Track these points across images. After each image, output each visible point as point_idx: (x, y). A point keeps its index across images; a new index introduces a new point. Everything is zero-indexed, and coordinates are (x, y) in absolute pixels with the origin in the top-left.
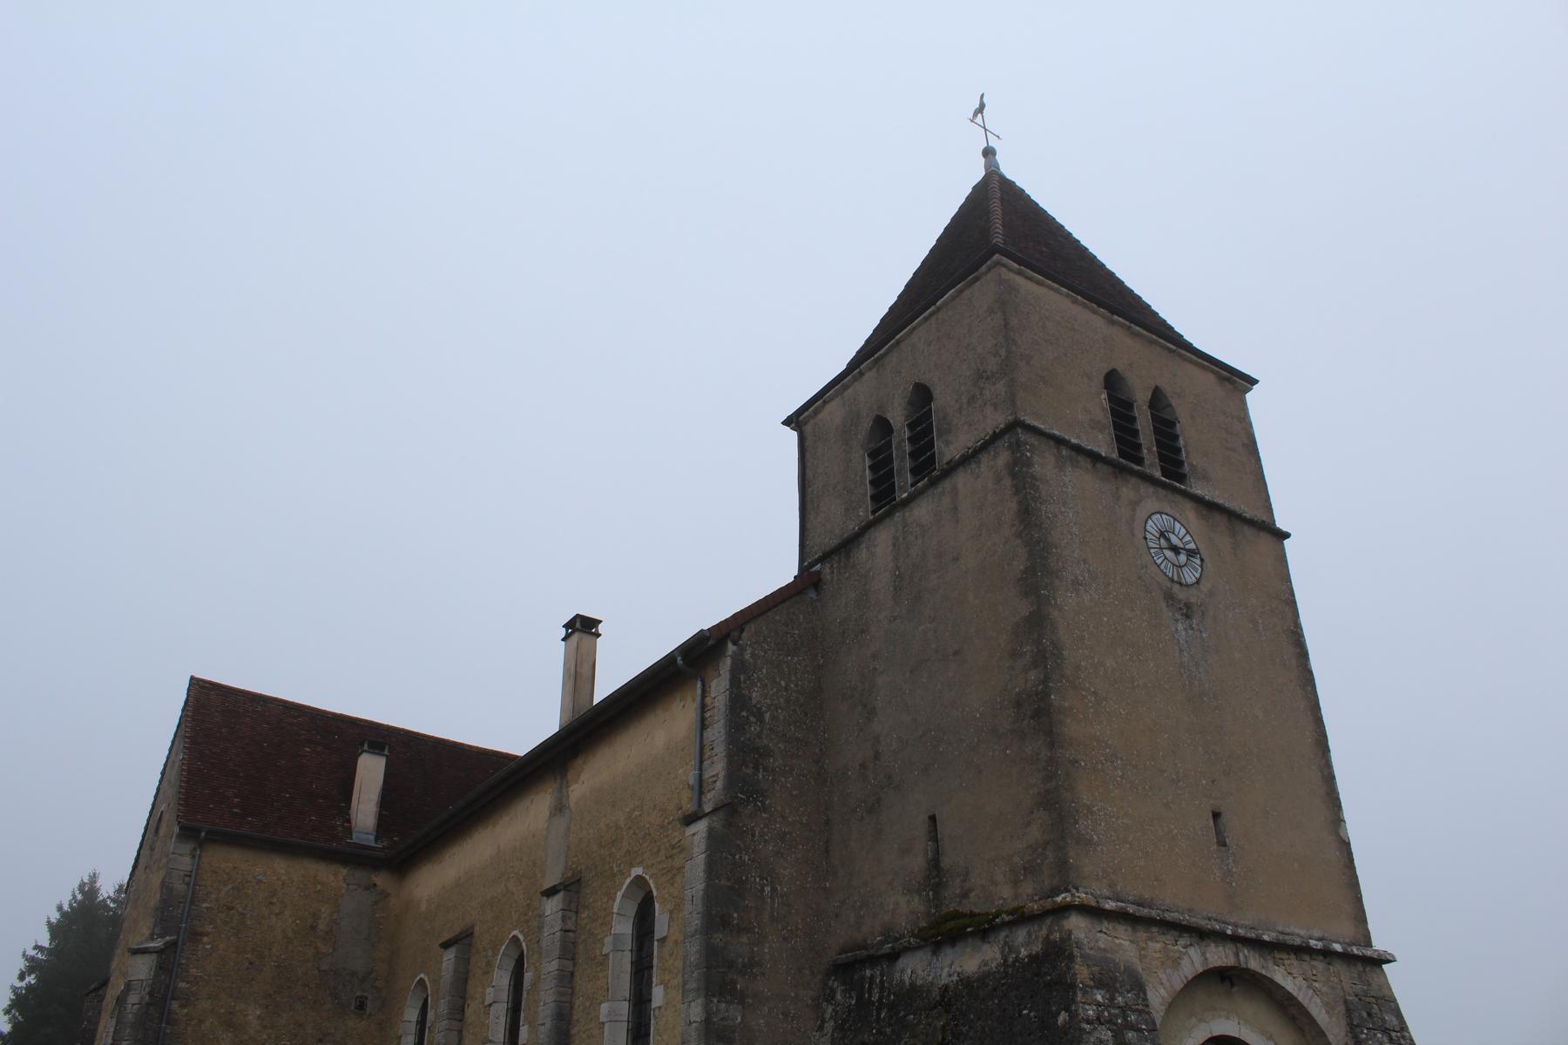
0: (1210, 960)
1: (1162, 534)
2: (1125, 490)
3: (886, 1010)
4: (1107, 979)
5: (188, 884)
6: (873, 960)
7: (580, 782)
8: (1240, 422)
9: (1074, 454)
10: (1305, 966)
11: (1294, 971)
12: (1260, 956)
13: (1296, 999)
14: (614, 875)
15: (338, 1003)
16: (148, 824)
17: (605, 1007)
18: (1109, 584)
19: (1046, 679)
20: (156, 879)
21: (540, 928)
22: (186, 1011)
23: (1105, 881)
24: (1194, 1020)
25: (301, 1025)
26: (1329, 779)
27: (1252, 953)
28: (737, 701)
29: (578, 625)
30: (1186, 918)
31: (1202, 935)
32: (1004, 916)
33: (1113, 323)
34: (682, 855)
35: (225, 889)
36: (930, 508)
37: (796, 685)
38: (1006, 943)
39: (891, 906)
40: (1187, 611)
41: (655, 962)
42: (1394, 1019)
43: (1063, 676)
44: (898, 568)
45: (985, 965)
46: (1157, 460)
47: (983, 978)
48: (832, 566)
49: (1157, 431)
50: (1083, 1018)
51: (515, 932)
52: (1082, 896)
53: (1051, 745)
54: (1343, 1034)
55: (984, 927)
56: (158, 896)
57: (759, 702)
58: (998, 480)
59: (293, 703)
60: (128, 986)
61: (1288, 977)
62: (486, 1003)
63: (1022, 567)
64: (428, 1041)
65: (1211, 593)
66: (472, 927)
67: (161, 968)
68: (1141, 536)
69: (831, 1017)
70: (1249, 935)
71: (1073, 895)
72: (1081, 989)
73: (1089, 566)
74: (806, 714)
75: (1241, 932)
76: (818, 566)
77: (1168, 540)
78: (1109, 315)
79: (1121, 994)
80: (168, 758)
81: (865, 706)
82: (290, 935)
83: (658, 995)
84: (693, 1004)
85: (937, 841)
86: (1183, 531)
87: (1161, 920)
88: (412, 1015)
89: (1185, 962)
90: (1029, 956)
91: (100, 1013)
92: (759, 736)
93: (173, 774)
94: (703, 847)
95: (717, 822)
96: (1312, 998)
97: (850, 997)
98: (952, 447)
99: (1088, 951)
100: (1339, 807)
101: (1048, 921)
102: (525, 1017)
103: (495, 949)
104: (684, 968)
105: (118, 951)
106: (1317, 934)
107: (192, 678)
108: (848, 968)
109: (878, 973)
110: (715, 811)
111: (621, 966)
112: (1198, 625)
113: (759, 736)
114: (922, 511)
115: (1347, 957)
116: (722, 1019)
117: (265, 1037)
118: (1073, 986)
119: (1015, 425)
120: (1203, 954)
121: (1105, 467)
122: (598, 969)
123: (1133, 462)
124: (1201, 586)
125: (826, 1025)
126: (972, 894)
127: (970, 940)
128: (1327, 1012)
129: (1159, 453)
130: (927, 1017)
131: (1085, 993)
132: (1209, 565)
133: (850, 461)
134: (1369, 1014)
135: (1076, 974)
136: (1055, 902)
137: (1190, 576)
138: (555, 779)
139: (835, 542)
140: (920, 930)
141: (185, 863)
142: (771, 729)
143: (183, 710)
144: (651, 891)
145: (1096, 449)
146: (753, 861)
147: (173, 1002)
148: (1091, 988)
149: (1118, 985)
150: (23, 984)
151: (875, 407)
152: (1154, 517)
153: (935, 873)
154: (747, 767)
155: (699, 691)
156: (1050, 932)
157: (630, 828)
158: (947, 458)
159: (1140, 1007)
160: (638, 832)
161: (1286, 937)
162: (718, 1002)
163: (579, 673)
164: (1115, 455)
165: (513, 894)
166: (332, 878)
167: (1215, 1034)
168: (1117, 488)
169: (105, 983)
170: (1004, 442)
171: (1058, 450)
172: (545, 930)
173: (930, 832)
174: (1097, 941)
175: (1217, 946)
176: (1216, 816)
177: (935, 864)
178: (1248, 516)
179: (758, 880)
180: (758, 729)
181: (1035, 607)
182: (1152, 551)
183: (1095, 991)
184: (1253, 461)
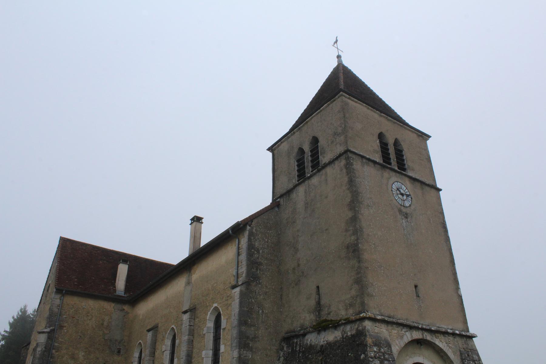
0: (414, 336)
1: (398, 189)
2: (385, 174)
3: (301, 354)
4: (378, 343)
5: (59, 309)
6: (297, 336)
7: (196, 274)
8: (425, 151)
10: (446, 338)
11: (442, 340)
12: (431, 335)
14: (207, 306)
17: (204, 353)
19: (357, 239)
20: (47, 307)
21: (182, 325)
22: (57, 353)
24: (408, 357)
26: (455, 274)
27: (428, 334)
28: (251, 247)
29: (195, 219)
30: (405, 322)
31: (411, 328)
32: (342, 321)
33: (381, 116)
34: (231, 299)
35: (72, 311)
37: (271, 241)
38: (343, 330)
39: (303, 318)
40: (406, 216)
41: (221, 337)
46: (396, 164)
47: (335, 343)
49: (396, 154)
51: (173, 326)
52: (369, 314)
53: (359, 262)
55: (335, 325)
56: (48, 313)
57: (258, 246)
58: (341, 170)
61: (440, 342)
62: (163, 351)
66: (158, 324)
68: (390, 190)
69: (282, 356)
70: (427, 328)
71: (366, 314)
72: (369, 346)
74: (274, 251)
75: (424, 327)
76: (279, 200)
77: (400, 191)
79: (383, 348)
80: (52, 265)
81: (295, 248)
82: (94, 327)
83: (222, 348)
84: (234, 351)
85: (319, 295)
86: (405, 188)
87: (397, 322)
88: (137, 355)
89: (405, 337)
90: (351, 335)
91: (27, 354)
92: (258, 258)
93: (54, 271)
94: (238, 297)
95: (243, 288)
97: (289, 349)
99: (371, 333)
104: (231, 339)
105: (34, 333)
106: (450, 327)
109: (299, 341)
110: (242, 284)
111: (210, 338)
113: (258, 258)
114: (315, 180)
115: (461, 336)
118: (366, 345)
119: (347, 151)
120: (411, 334)
122: (201, 339)
123: (387, 164)
125: (281, 359)
126: (332, 314)
127: (331, 329)
128: (454, 355)
130: (316, 356)
131: (370, 348)
134: (468, 355)
135: (367, 341)
136: (360, 316)
137: (407, 204)
139: (285, 191)
140: (314, 326)
141: (58, 302)
143: (58, 248)
144: (220, 312)
145: (375, 160)
148: (372, 346)
149: (382, 345)
151: (299, 144)
152: (395, 183)
153: (319, 306)
155: (237, 243)
156: (358, 327)
158: (323, 162)
159: (389, 353)
162: (243, 350)
163: (196, 236)
164: (382, 162)
166: (109, 307)
168: (382, 173)
170: (343, 157)
172: (183, 325)
173: (317, 292)
174: (374, 330)
175: (416, 332)
176: (416, 287)
177: (319, 303)
178: (427, 183)
179: (257, 308)
180: (258, 256)
182: (394, 195)
183: (374, 347)
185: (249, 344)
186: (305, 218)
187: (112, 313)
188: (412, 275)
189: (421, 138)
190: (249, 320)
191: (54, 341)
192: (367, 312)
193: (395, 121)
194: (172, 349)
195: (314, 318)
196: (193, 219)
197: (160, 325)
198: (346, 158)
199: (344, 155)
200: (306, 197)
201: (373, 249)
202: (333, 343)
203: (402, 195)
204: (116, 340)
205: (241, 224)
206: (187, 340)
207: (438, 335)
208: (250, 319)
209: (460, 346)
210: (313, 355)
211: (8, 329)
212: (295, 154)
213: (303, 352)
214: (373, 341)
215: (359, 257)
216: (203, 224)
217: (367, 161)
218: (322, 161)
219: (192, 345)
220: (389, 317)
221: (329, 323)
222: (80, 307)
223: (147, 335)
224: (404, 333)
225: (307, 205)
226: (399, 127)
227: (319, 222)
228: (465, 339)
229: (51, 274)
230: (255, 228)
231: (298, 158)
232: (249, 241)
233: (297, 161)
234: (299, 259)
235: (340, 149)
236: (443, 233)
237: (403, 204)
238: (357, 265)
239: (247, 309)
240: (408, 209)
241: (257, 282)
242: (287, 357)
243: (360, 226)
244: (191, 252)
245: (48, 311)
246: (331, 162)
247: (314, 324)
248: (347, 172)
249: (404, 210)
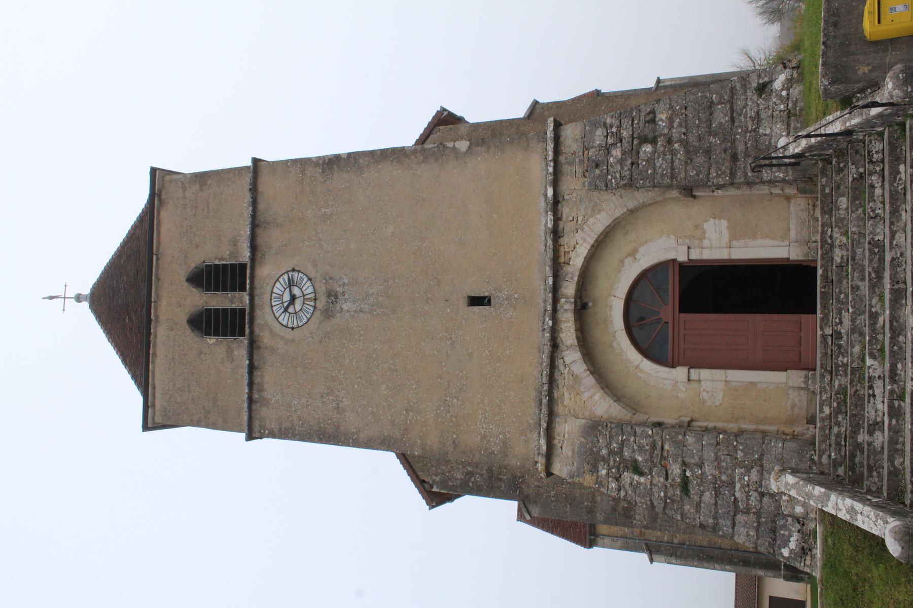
11: (572, 243)
24: (614, 344)
33: (157, 317)
40: (333, 296)
50: (617, 494)
57: (462, 474)
78: (153, 323)
113: (482, 476)
116: (645, 518)
146: (554, 488)
154: (501, 487)
162: (635, 520)
167: (624, 328)
179: (564, 486)
185: (623, 507)
189: (164, 196)
190: (586, 503)
193: (153, 278)
207: (563, 254)
208: (583, 503)
226: (160, 262)
239: (568, 506)
241: (522, 481)
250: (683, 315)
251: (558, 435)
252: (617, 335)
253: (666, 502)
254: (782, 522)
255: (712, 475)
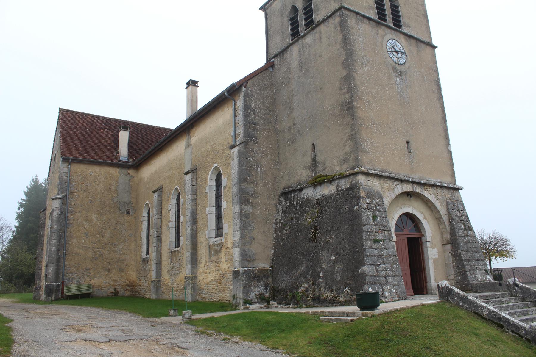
0: (404, 189)
1: (393, 47)
2: (380, 31)
3: (299, 207)
4: (370, 195)
5: (67, 177)
6: (294, 191)
7: (195, 136)
8: (422, 6)
9: (362, 18)
10: (435, 191)
11: (431, 192)
12: (420, 188)
13: (431, 201)
14: (208, 167)
15: (121, 212)
16: (51, 158)
17: (207, 209)
18: (373, 64)
19: (352, 97)
20: (57, 176)
21: (185, 185)
22: (72, 216)
23: (370, 164)
24: (398, 208)
25: (110, 219)
26: (446, 130)
27: (418, 187)
28: (247, 107)
29: (191, 83)
30: (397, 176)
31: (402, 181)
32: (337, 176)
34: (230, 159)
35: (80, 178)
36: (311, 38)
37: (266, 101)
38: (338, 184)
39: (300, 174)
40: (400, 74)
41: (223, 194)
42: (461, 207)
43: (357, 96)
44: (301, 59)
45: (331, 192)
46: (392, 20)
47: (330, 196)
48: (278, 60)
49: (392, 10)
51: (177, 187)
52: (363, 169)
53: (353, 119)
54: (445, 212)
55: (331, 180)
56: (58, 181)
58: (335, 28)
59: (95, 115)
60: (53, 209)
61: (429, 194)
62: (169, 210)
63: (343, 59)
64: (151, 223)
65: (409, 68)
66: (162, 186)
67: (62, 204)
68: (385, 47)
69: (281, 210)
70: (417, 181)
71: (360, 169)
72: (362, 199)
73: (367, 58)
74: (270, 111)
75: (414, 180)
76: (273, 60)
77: (395, 49)
79: (375, 200)
80: (55, 136)
81: (290, 107)
82: (103, 191)
83: (224, 205)
84: (236, 207)
85: (315, 152)
86: (400, 46)
87: (389, 176)
88: (145, 214)
89: (396, 190)
90: (345, 189)
91: (45, 218)
92: (254, 118)
93: (58, 141)
94: (237, 156)
95: (241, 147)
96: (436, 200)
97: (287, 203)
98: (319, 16)
99: (364, 187)
100: (449, 140)
101: (352, 177)
102: (182, 214)
103: (170, 193)
104: (232, 196)
105: (48, 199)
106: (439, 181)
107: (60, 109)
108: (285, 194)
109: (296, 195)
110: (240, 144)
111: (212, 196)
112: (404, 78)
113: (254, 118)
114: (309, 39)
115: (448, 188)
116: (245, 211)
117: (99, 223)
118: (359, 198)
119: (341, 8)
120: (402, 187)
121: (373, 23)
122: (204, 197)
123: (383, 21)
124: (406, 65)
125: (279, 212)
126: (327, 169)
127: (326, 184)
128: (441, 205)
129: (392, 17)
130: (312, 208)
131: (363, 200)
132: (409, 58)
133: (283, 22)
134: (454, 205)
135: (360, 194)
136: (354, 171)
137: (402, 61)
138: (186, 136)
139: (278, 51)
140: (310, 181)
141: (66, 170)
142: (258, 116)
143: (58, 119)
144: (220, 171)
145: (370, 16)
146: (254, 160)
147: (68, 214)
148: (365, 198)
149: (374, 197)
150: (20, 211)
151: (292, 2)
152: (390, 41)
153: (314, 162)
155: (233, 104)
156: (352, 181)
157: (212, 151)
158: (317, 20)
159: (381, 204)
160: (215, 152)
161: (429, 182)
163: (192, 100)
164: (377, 19)
165: (175, 174)
166: (115, 172)
168: (377, 30)
169: (45, 209)
170: (337, 14)
171: (357, 17)
172: (186, 185)
173: (312, 149)
174: (367, 183)
175: (406, 185)
176: (408, 143)
177: (314, 160)
178: (423, 40)
179: (255, 166)
180: (254, 116)
181: (348, 72)
182: (389, 52)
183: (367, 199)
184: (426, 20)
185: (250, 199)
186: (300, 77)
187: (119, 178)
188: (404, 131)
191: (68, 206)
192: (360, 167)
194: (178, 208)
195: (310, 174)
196: (188, 83)
197: (164, 187)
198: (340, 15)
199: (338, 12)
200: (300, 56)
201: (367, 107)
202: (329, 196)
203: (397, 52)
204: (125, 203)
205: (236, 85)
206: (191, 199)
209: (447, 197)
210: (310, 208)
211: (24, 197)
212: (288, 12)
213: (301, 206)
214: (365, 194)
215: (353, 115)
216: (198, 88)
217: (362, 18)
218: (315, 18)
219: (195, 203)
220: (382, 172)
221: (325, 178)
222: (87, 174)
223: (153, 196)
224: (396, 186)
225: (301, 65)
227: (314, 81)
228: (452, 191)
229: (55, 144)
230: (250, 89)
231: (291, 16)
232: (244, 101)
233: (290, 20)
234: (294, 118)
235: (335, 6)
236: (436, 91)
237: (398, 62)
238: (351, 122)
240: (403, 66)
242: (285, 211)
243: (354, 85)
244: (189, 116)
245: (58, 179)
246: (324, 20)
247: (310, 179)
248: (341, 30)
249: (398, 68)
250: (406, 239)
251: (373, 179)
252: (401, 210)
253: (368, 232)
254: (379, 287)
255: (384, 254)
